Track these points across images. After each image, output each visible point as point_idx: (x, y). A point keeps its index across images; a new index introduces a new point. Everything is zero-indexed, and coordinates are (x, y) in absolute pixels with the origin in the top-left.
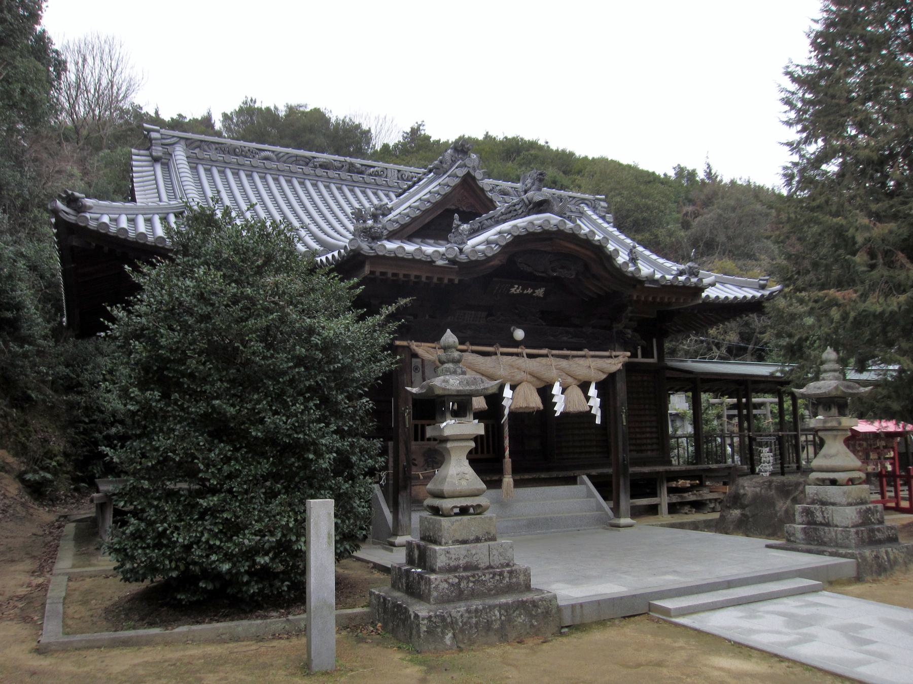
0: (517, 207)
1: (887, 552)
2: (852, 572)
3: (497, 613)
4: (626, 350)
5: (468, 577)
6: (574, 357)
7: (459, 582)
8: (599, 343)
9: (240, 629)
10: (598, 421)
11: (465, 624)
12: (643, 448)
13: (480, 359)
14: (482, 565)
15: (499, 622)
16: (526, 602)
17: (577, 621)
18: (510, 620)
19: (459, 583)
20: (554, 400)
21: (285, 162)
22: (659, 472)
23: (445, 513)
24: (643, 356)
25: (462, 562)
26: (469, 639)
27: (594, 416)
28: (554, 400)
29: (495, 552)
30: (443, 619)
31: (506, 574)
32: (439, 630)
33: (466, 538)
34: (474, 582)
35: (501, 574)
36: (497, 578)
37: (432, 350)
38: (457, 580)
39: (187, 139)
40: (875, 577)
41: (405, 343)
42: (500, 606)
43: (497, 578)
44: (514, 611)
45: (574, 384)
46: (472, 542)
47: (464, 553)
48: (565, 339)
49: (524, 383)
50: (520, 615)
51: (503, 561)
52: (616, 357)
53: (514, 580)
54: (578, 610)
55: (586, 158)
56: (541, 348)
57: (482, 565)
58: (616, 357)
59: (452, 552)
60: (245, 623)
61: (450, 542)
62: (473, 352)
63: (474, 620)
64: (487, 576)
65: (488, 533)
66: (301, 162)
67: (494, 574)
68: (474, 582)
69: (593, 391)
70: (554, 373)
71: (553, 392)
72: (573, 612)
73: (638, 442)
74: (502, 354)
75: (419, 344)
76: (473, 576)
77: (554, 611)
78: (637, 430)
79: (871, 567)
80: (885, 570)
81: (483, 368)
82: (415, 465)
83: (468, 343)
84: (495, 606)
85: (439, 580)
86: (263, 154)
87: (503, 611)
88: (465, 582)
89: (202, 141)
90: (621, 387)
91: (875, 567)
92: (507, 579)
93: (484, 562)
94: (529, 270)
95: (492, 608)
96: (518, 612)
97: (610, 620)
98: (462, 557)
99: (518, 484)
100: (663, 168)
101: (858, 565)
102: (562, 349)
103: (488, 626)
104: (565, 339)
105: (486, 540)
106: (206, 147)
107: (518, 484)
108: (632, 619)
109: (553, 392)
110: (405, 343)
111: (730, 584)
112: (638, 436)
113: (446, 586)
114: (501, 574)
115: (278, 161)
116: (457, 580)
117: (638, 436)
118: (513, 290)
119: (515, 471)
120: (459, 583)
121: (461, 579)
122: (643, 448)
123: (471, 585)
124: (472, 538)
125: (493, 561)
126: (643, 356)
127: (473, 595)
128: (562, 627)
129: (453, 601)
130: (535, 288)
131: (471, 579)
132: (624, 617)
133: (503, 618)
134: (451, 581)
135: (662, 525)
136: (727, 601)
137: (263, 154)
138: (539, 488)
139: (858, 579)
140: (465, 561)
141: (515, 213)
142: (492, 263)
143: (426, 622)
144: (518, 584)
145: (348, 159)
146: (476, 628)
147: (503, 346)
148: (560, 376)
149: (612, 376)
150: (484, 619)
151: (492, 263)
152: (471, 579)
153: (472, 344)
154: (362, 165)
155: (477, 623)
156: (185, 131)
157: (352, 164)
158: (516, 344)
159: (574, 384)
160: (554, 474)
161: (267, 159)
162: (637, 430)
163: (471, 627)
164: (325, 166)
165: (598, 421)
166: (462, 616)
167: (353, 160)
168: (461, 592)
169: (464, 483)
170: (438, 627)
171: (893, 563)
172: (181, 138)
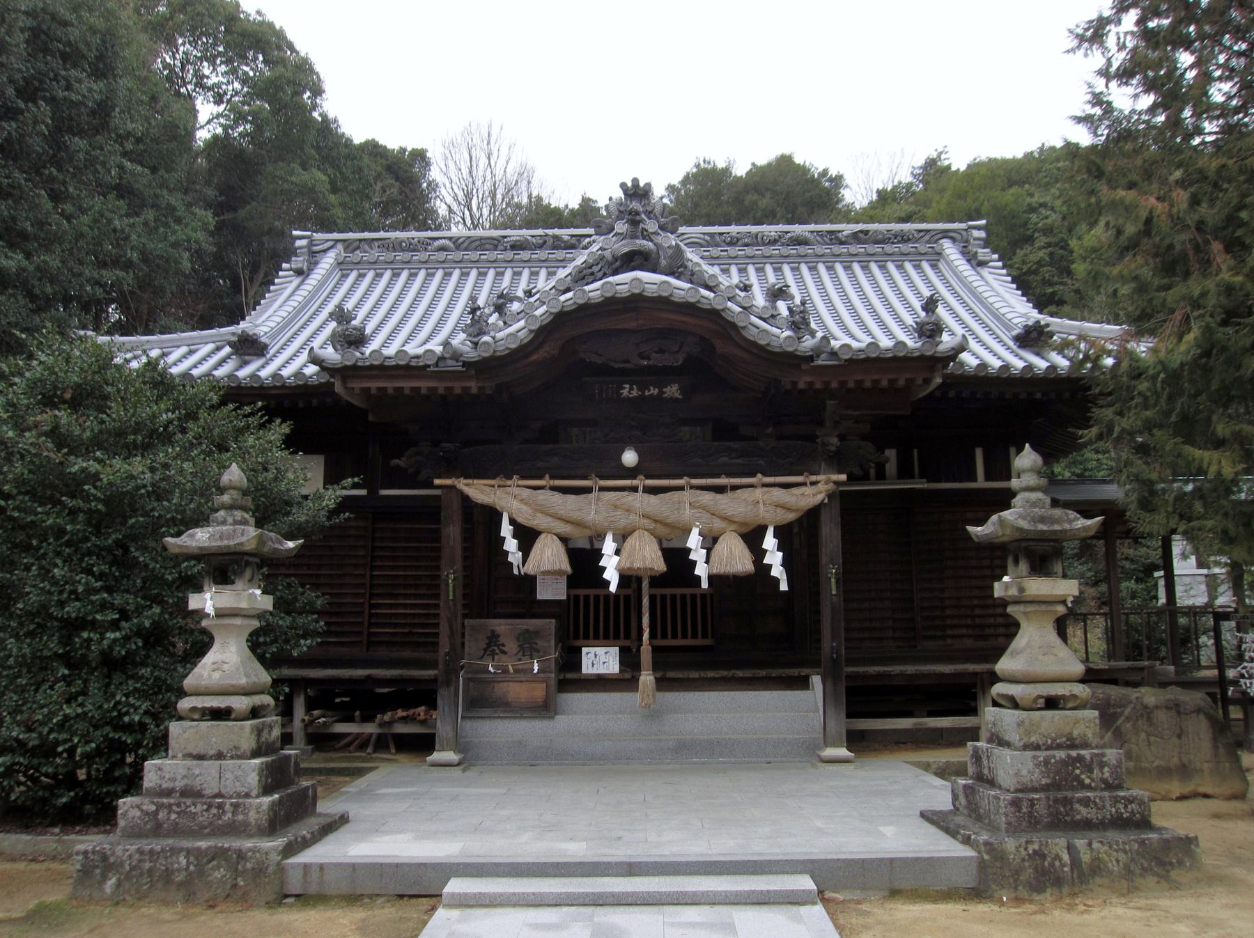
0: (595, 269)
1: (1070, 848)
2: (967, 879)
3: (183, 861)
4: (840, 472)
5: (170, 805)
6: (735, 488)
7: (157, 811)
8: (787, 461)
9: (6, 843)
10: (784, 586)
11: (133, 868)
12: (988, 631)
13: (557, 498)
14: (208, 792)
15: (184, 873)
16: (229, 849)
17: (313, 889)
18: (201, 873)
19: (156, 812)
20: (692, 557)
21: (466, 250)
22: (975, 674)
23: (183, 714)
24: (988, 478)
25: (179, 784)
26: (138, 891)
27: (776, 581)
28: (692, 557)
29: (228, 775)
30: (104, 858)
31: (227, 807)
32: (98, 871)
33: (202, 752)
34: (178, 813)
35: (220, 806)
36: (214, 811)
37: (487, 489)
38: (154, 808)
39: (344, 241)
40: (1022, 892)
41: (448, 482)
42: (189, 852)
43: (214, 811)
44: (210, 862)
45: (729, 528)
46: (211, 758)
47: (183, 771)
48: (724, 459)
49: (636, 533)
50: (218, 867)
51: (240, 789)
52: (813, 483)
53: (241, 817)
54: (315, 875)
55: (1029, 156)
56: (680, 477)
57: (208, 792)
58: (813, 483)
59: (166, 769)
60: (25, 837)
61: (180, 755)
62: (553, 488)
63: (147, 865)
64: (199, 806)
65: (236, 748)
66: (487, 246)
67: (210, 806)
68: (178, 813)
69: (770, 542)
70: (688, 512)
71: (764, 546)
72: (305, 874)
73: (977, 621)
74: (602, 489)
75: (470, 481)
76: (178, 805)
77: (271, 869)
78: (976, 602)
79: (1017, 873)
80: (1058, 882)
81: (562, 512)
82: (504, 653)
83: (759, 475)
84: (181, 850)
85: (128, 805)
86: (437, 244)
87: (192, 859)
88: (166, 811)
89: (360, 240)
90: (830, 534)
91: (1028, 874)
92: (230, 815)
93: (211, 787)
94: (599, 361)
95: (175, 851)
96: (215, 863)
97: (371, 897)
98: (179, 777)
99: (663, 684)
100: (1020, 155)
101: (982, 866)
102: (718, 476)
103: (168, 875)
104: (724, 459)
105: (232, 758)
106: (366, 247)
107: (663, 684)
108: (414, 901)
109: (764, 546)
110: (448, 482)
111: (631, 869)
112: (977, 612)
113: (138, 814)
114: (220, 806)
115: (458, 248)
116: (154, 808)
117: (977, 612)
118: (625, 392)
119: (656, 667)
120: (156, 812)
121: (160, 807)
122: (988, 631)
123: (173, 816)
124: (212, 752)
125: (225, 786)
126: (988, 478)
127: (176, 831)
128: (286, 896)
129: (147, 837)
130: (661, 386)
131: (174, 808)
132: (401, 896)
133: (192, 868)
134: (145, 807)
135: (911, 763)
136: (568, 895)
137: (437, 244)
138: (726, 693)
139: (977, 893)
140: (183, 783)
141: (592, 278)
142: (534, 357)
143: (80, 857)
144: (246, 824)
145: (550, 232)
146: (150, 876)
147: (602, 477)
148: (698, 519)
149: (813, 514)
150: (161, 864)
151: (534, 357)
152: (174, 808)
153: (552, 477)
154: (572, 236)
155: (150, 871)
156: (375, 231)
157: (556, 237)
158: (631, 473)
159: (729, 528)
160: (774, 673)
161: (443, 249)
162: (976, 602)
163: (141, 875)
164: (517, 246)
165: (784, 586)
166: (130, 857)
167: (557, 231)
168: (159, 825)
169: (216, 675)
170: (97, 867)
171: (1097, 868)
172: (337, 241)
